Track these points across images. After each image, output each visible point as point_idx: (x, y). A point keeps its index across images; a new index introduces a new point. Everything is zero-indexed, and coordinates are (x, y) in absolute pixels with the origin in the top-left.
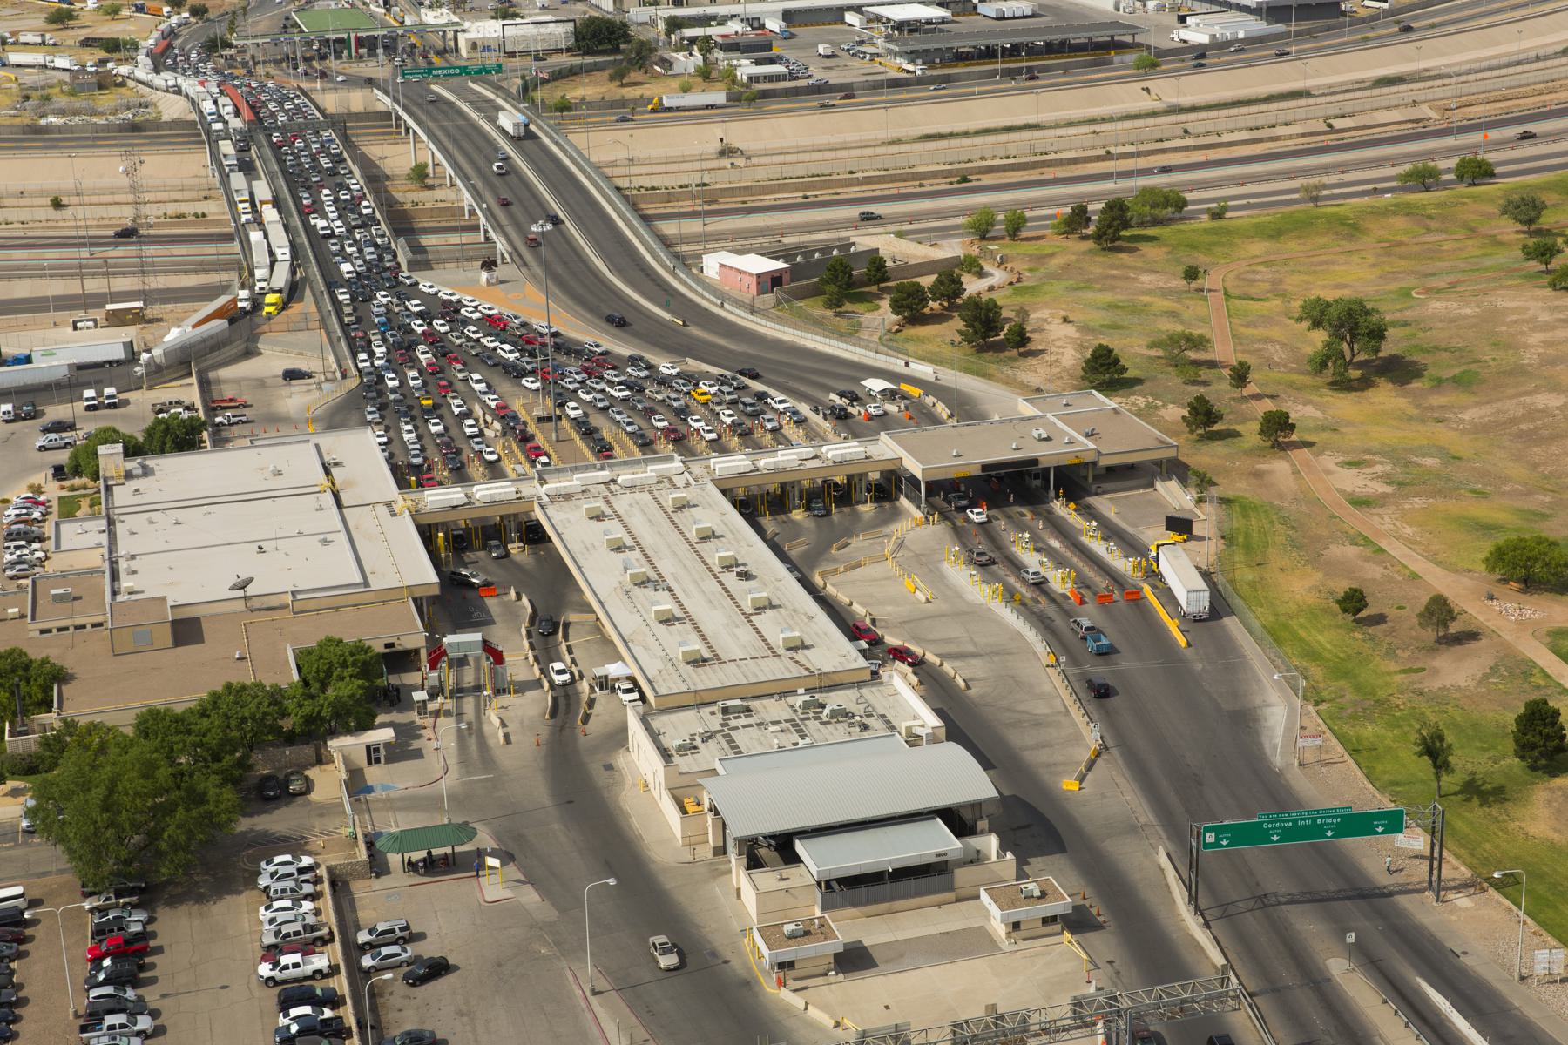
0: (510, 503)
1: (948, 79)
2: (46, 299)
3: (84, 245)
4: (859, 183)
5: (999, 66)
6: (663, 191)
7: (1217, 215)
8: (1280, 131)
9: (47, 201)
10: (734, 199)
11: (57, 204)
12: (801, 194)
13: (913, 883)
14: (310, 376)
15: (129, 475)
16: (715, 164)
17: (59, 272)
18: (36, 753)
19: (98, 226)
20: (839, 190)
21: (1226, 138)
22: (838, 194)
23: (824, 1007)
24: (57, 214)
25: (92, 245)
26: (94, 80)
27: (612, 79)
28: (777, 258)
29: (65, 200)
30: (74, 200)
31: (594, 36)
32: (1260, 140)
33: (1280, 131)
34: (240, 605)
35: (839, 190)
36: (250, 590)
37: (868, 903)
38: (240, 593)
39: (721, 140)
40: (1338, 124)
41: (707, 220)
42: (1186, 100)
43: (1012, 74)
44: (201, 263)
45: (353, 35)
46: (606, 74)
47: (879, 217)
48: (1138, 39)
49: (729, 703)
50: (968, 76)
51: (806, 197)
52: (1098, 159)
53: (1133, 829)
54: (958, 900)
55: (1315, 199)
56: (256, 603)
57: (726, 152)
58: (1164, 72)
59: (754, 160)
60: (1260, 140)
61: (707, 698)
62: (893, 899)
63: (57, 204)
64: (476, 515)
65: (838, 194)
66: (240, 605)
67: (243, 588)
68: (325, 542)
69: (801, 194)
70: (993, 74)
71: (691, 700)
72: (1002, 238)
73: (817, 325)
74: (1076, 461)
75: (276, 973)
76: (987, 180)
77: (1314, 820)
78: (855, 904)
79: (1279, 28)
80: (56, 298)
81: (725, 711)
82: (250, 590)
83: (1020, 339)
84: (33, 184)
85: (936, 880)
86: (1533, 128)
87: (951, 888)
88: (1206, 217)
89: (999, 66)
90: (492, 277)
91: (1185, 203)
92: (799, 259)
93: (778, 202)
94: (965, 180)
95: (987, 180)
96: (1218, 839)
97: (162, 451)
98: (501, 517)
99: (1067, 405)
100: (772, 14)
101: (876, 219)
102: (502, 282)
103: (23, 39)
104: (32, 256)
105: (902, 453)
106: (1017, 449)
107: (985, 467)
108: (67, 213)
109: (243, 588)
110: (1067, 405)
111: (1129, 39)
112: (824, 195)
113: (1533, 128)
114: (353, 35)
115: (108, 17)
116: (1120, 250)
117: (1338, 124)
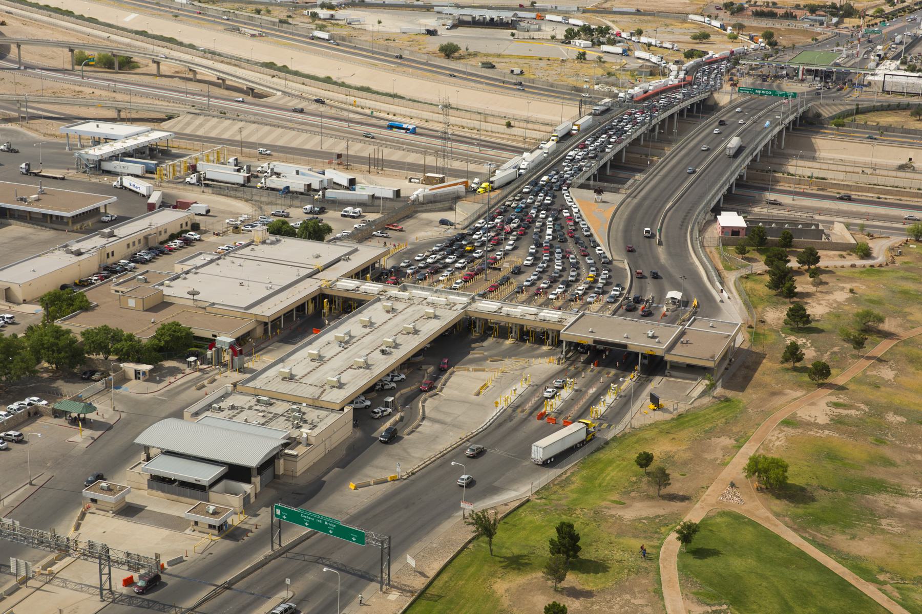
0: (553, 323)
2: (404, 163)
6: (797, 177)
9: (504, 122)
10: (834, 190)
11: (509, 125)
12: (876, 196)
13: (188, 491)
14: (452, 224)
15: (264, 242)
16: (894, 173)
19: (508, 139)
20: (902, 198)
22: (901, 200)
26: (649, 70)
27: (912, 115)
35: (902, 198)
36: (196, 297)
37: (168, 492)
38: (191, 297)
39: (910, 159)
41: (796, 197)
45: (801, 68)
46: (909, 112)
47: (780, 204)
49: (262, 398)
51: (879, 198)
56: (199, 304)
58: (846, 132)
59: (878, 171)
62: (179, 495)
63: (509, 125)
64: (500, 319)
65: (901, 200)
66: (191, 303)
67: (194, 295)
68: (241, 284)
69: (876, 196)
74: (651, 353)
77: (324, 521)
78: (163, 491)
80: (409, 164)
81: (258, 401)
85: (199, 493)
90: (599, 198)
92: (773, 225)
93: (860, 198)
96: (282, 515)
97: (301, 237)
98: (512, 324)
99: (712, 327)
101: (777, 204)
102: (604, 202)
103: (664, 45)
104: (429, 142)
106: (627, 338)
107: (596, 341)
109: (194, 295)
110: (712, 327)
112: (891, 199)
114: (801, 68)
115: (731, 40)
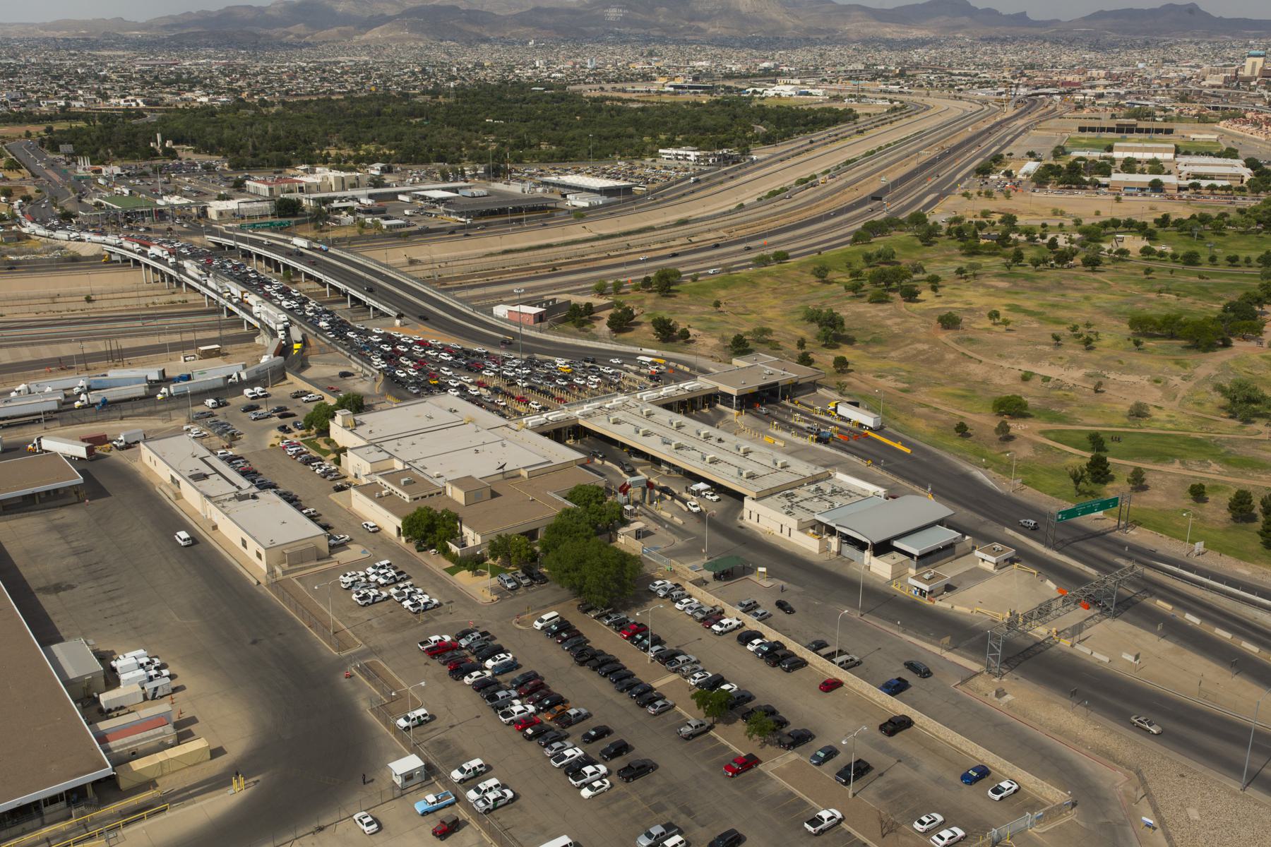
1: (487, 225)
3: (139, 319)
4: (508, 272)
5: (509, 218)
7: (694, 280)
8: (672, 243)
9: (83, 298)
11: (89, 300)
17: (172, 331)
18: (1092, 458)
21: (653, 247)
23: (962, 604)
24: (91, 305)
25: (143, 319)
28: (534, 306)
29: (93, 297)
30: (99, 297)
31: (286, 208)
32: (666, 248)
33: (672, 243)
34: (500, 477)
36: (506, 468)
38: (501, 471)
40: (694, 239)
42: (605, 232)
43: (520, 221)
44: (208, 325)
48: (558, 206)
50: (496, 223)
52: (605, 258)
53: (983, 523)
54: (957, 558)
55: (729, 270)
56: (507, 475)
57: (412, 262)
60: (666, 248)
61: (774, 491)
63: (89, 300)
68: (477, 451)
70: (507, 222)
71: (767, 493)
72: (610, 293)
73: (575, 336)
75: (723, 629)
76: (564, 269)
79: (614, 199)
80: (170, 344)
82: (506, 468)
83: (685, 335)
84: (75, 289)
86: (751, 244)
87: (954, 554)
88: (689, 281)
89: (509, 218)
91: (680, 274)
94: (555, 269)
95: (564, 269)
100: (363, 196)
105: (716, 384)
108: (96, 304)
111: (553, 205)
113: (751, 244)
116: (670, 296)
117: (694, 239)
